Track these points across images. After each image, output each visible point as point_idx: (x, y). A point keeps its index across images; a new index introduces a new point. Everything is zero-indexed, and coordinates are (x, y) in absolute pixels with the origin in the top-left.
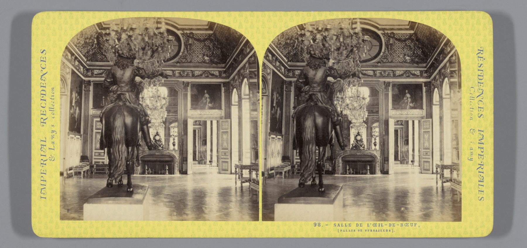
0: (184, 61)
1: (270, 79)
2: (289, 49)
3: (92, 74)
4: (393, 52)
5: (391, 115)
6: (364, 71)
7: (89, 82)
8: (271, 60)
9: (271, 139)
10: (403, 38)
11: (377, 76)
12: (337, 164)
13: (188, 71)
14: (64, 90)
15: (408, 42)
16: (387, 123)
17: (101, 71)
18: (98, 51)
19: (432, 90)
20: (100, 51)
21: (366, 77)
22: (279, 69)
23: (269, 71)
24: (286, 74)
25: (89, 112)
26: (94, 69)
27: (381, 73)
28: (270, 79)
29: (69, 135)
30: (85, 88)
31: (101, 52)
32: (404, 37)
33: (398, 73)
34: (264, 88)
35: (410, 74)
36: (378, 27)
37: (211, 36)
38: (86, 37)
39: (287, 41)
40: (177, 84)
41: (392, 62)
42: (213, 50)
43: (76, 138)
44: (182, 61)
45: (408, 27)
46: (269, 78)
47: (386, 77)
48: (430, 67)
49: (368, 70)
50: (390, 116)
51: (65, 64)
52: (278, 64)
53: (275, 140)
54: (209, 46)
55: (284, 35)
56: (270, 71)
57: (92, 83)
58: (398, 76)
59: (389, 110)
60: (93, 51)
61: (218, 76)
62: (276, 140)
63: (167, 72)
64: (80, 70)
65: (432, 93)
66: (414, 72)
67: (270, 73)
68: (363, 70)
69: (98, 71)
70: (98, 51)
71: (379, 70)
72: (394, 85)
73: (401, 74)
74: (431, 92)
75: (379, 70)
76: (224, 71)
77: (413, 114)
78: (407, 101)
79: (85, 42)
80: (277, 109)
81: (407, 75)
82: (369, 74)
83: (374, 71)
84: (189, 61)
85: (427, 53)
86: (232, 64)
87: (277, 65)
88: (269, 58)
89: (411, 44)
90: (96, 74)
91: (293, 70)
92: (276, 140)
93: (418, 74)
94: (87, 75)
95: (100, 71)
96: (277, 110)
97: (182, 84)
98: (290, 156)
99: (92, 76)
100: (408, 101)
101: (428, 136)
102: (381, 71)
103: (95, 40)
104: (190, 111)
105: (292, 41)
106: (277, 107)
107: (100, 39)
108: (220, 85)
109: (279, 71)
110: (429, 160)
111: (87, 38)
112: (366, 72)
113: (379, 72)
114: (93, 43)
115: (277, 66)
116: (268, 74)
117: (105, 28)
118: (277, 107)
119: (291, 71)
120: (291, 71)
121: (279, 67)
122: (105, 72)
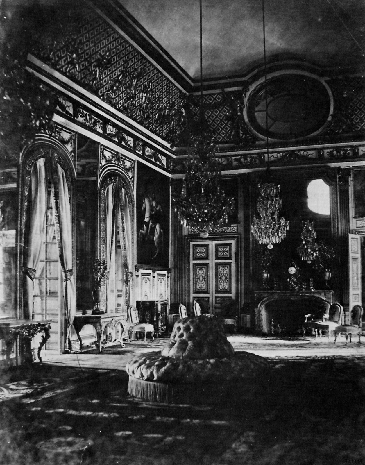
1: (133, 177)
6: (302, 152)
9: (140, 277)
12: (257, 316)
22: (153, 160)
25: (351, 225)
27: (331, 153)
29: (137, 270)
43: (156, 275)
46: (131, 176)
50: (352, 230)
53: (151, 277)
59: (351, 219)
62: (154, 277)
71: (328, 148)
75: (328, 148)
80: (155, 227)
92: (154, 277)
95: (279, 155)
96: (153, 229)
102: (331, 150)
103: (183, 110)
104: (355, 220)
106: (155, 223)
110: (57, 313)
112: (305, 153)
113: (329, 150)
118: (155, 223)
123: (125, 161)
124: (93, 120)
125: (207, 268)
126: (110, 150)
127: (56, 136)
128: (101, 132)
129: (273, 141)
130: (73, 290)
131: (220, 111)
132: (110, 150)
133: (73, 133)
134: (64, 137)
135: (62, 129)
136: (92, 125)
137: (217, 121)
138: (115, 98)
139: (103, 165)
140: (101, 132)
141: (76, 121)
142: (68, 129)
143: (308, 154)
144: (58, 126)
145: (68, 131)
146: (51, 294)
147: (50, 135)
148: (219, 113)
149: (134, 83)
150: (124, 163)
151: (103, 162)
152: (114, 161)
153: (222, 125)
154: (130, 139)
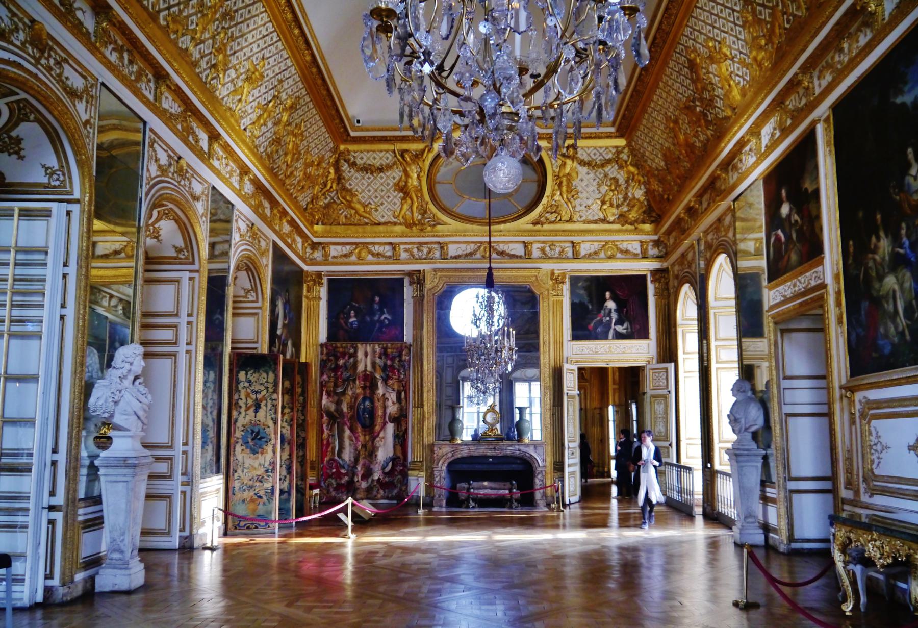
0: (553, 220)
2: (315, 193)
3: (326, 255)
4: (573, 197)
5: (570, 355)
6: (377, 247)
7: (319, 275)
8: (269, 215)
10: (598, 159)
11: (533, 256)
13: (562, 245)
14: (254, 294)
15: (612, 170)
16: (558, 375)
17: (348, 247)
18: (338, 198)
19: (672, 291)
20: (344, 198)
21: (382, 259)
22: (289, 241)
23: (263, 244)
24: (308, 254)
26: (329, 244)
28: (267, 265)
30: (308, 291)
31: (347, 201)
32: (601, 157)
33: (584, 249)
34: (252, 289)
35: (615, 250)
36: (386, 137)
37: (622, 152)
38: (308, 161)
39: (308, 171)
40: (536, 276)
41: (570, 220)
42: (627, 188)
44: (547, 219)
45: (612, 130)
46: (265, 263)
47: (557, 258)
48: (668, 233)
49: (512, 242)
51: (255, 228)
52: (286, 228)
54: (615, 180)
55: (300, 153)
56: (268, 244)
57: (325, 280)
58: (585, 256)
60: (326, 198)
61: (637, 254)
63: (512, 246)
64: (294, 246)
65: (672, 298)
66: (625, 246)
67: (268, 251)
68: (373, 244)
69: (339, 248)
70: (338, 198)
72: (575, 280)
73: (468, 251)
74: (669, 296)
76: (654, 241)
77: (623, 353)
78: (608, 319)
79: (305, 173)
81: (609, 253)
82: (512, 253)
83: (526, 245)
84: (565, 218)
85: (662, 196)
86: (679, 221)
87: (284, 231)
88: (263, 211)
89: (618, 173)
90: (334, 257)
91: (324, 246)
93: (635, 252)
94: (311, 260)
95: (344, 249)
97: (549, 275)
98: (543, 460)
99: (326, 262)
100: (611, 319)
101: (662, 406)
103: (332, 171)
105: (321, 172)
107: (343, 169)
108: (402, 280)
109: (289, 246)
111: (311, 164)
114: (327, 177)
115: (284, 233)
116: (263, 253)
117: (354, 137)
119: (320, 248)
120: (320, 248)
121: (289, 235)
122: (357, 251)
123: (193, 180)
124: (229, 168)
125: (171, 465)
126: (165, 148)
127: (185, 185)
128: (151, 98)
129: (585, 542)
130: (602, 532)
131: (388, 177)
132: (165, 148)
133: (206, 185)
134: (75, 87)
135: (193, 176)
136: (133, 78)
137: (382, 191)
138: (259, 137)
139: (153, 176)
140: (151, 98)
141: (211, 164)
142: (167, 144)
143: (511, 248)
144: (55, 47)
145: (80, 70)
146: (49, 468)
147: (38, 61)
148: (386, 180)
149: (285, 118)
150: (259, 242)
151: (154, 170)
152: (173, 174)
153: (388, 197)
154: (203, 137)
